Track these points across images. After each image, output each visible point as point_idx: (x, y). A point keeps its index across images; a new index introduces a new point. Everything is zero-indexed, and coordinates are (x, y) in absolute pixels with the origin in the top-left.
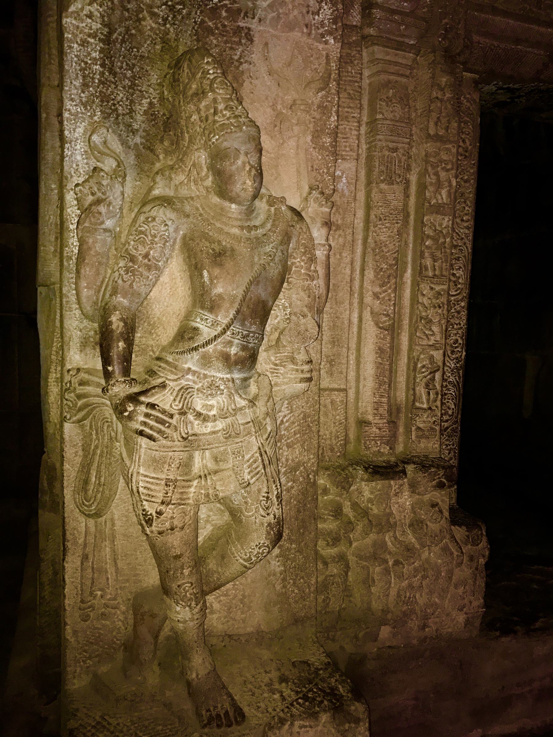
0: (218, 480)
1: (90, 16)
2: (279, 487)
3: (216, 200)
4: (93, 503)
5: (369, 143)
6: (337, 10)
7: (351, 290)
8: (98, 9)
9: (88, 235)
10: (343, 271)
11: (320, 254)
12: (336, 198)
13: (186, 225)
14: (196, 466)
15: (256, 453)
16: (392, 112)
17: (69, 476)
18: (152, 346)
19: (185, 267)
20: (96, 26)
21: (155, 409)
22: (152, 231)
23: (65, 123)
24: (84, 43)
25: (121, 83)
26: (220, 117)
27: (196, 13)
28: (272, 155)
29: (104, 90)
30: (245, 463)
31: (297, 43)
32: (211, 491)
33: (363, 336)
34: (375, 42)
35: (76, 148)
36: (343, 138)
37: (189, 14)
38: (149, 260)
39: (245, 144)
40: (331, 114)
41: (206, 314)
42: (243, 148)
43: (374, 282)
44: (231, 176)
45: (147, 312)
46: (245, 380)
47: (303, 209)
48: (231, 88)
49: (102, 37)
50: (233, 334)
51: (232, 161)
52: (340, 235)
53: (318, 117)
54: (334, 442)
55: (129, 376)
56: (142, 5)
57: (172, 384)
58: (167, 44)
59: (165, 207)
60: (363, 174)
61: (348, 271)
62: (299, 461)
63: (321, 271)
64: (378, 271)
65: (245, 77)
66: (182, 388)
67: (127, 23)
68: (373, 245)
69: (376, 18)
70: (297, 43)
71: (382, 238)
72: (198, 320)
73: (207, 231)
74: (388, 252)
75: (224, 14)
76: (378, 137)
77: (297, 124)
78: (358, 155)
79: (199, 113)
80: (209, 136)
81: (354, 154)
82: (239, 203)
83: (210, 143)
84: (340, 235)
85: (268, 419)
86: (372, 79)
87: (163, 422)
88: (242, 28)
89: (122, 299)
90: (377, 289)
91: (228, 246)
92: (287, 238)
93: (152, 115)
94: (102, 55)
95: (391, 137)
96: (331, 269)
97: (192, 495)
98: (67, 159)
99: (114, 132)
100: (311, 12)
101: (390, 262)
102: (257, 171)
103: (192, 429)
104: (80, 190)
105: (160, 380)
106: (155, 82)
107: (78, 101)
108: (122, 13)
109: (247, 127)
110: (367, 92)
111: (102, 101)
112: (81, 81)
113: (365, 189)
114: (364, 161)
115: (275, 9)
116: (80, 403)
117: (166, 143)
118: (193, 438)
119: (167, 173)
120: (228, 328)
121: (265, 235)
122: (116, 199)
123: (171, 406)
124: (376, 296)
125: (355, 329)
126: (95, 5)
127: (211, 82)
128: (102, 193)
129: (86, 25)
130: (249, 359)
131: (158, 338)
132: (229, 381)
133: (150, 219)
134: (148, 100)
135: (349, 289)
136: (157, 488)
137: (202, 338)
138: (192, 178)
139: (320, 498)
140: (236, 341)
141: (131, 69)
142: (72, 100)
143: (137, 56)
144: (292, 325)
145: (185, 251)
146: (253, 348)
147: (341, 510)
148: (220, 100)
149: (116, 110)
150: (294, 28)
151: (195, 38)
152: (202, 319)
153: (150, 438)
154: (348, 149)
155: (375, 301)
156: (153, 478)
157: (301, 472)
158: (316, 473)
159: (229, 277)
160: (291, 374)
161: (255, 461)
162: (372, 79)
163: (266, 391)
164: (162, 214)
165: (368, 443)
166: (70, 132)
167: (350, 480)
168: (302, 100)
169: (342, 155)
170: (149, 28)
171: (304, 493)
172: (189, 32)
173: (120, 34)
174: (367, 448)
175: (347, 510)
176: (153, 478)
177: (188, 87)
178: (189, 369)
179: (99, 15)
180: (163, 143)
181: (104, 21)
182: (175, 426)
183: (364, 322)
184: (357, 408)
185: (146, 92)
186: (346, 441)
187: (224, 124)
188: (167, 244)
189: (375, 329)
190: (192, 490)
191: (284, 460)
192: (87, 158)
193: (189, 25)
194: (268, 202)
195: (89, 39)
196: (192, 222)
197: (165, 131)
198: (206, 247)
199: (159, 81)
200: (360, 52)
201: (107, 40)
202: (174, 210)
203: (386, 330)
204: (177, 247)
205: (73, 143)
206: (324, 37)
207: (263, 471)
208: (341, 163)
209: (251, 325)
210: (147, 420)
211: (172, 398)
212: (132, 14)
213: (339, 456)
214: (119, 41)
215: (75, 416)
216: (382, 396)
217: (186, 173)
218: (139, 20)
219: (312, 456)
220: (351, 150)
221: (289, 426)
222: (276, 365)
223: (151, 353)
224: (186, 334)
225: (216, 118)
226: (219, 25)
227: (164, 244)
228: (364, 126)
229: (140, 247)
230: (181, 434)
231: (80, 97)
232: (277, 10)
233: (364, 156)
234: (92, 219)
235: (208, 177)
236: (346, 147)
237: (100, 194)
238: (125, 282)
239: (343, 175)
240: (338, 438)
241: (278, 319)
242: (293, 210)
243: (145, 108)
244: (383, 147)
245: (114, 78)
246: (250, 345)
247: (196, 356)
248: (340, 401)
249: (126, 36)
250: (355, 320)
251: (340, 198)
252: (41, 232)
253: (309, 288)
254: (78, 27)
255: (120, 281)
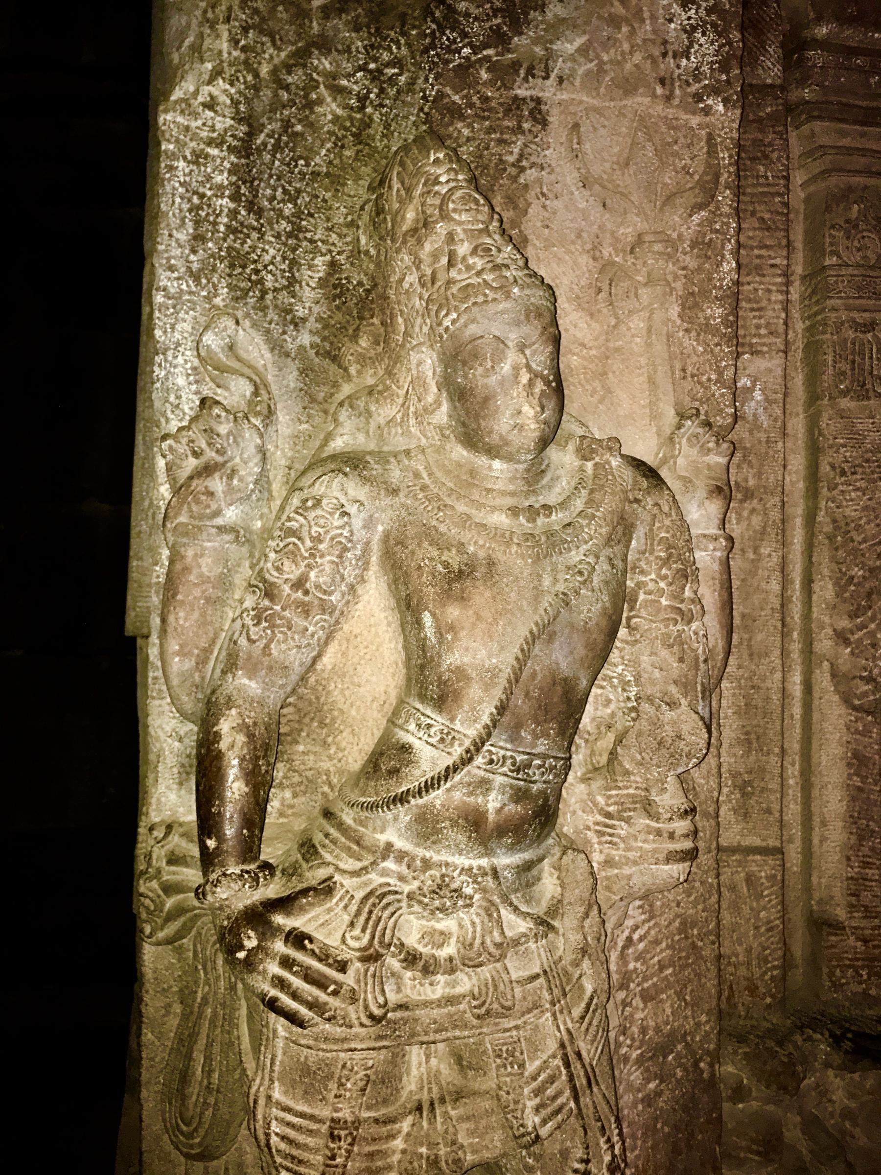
0: (461, 1119)
1: (211, 105)
2: (615, 1139)
3: (459, 452)
4: (196, 1130)
5: (809, 318)
6: (729, 43)
7: (783, 625)
8: (226, 91)
9: (185, 540)
10: (763, 585)
11: (706, 558)
12: (741, 432)
13: (390, 512)
14: (414, 1072)
15: (554, 1056)
16: (859, 250)
17: (152, 1059)
18: (328, 773)
19: (393, 603)
20: (223, 123)
21: (303, 948)
22: (315, 529)
23: (157, 314)
24: (198, 158)
25: (272, 229)
26: (460, 272)
27: (426, 80)
28: (593, 352)
29: (237, 245)
30: (528, 1083)
31: (642, 119)
32: (443, 1151)
33: (815, 728)
34: (815, 113)
35: (175, 362)
36: (752, 310)
37: (412, 82)
38: (306, 593)
39: (518, 325)
40: (723, 256)
41: (428, 712)
42: (513, 336)
43: (835, 607)
44: (486, 400)
45: (317, 698)
46: (528, 866)
47: (664, 461)
48: (486, 209)
49: (235, 143)
50: (491, 762)
51: (490, 364)
52: (753, 511)
53: (693, 264)
54: (757, 972)
55: (256, 858)
56: (314, 75)
57: (348, 882)
58: (368, 145)
59: (345, 474)
60: (798, 381)
61: (775, 586)
62: (673, 1031)
63: (710, 597)
64: (843, 583)
65: (531, 195)
66: (371, 893)
67: (286, 112)
68: (828, 529)
69: (815, 66)
70: (642, 119)
71: (848, 512)
72: (412, 727)
73: (434, 523)
74: (865, 541)
75: (484, 75)
76: (830, 303)
77: (646, 285)
78: (787, 343)
79: (418, 268)
80: (437, 316)
81: (779, 342)
82: (509, 458)
83: (441, 330)
84: (753, 511)
85: (586, 964)
86: (812, 188)
87: (320, 983)
88: (524, 99)
89: (245, 681)
90: (844, 623)
91: (482, 554)
92: (622, 529)
93: (335, 287)
94: (234, 179)
95: (858, 302)
96: (736, 583)
97: (396, 1157)
98: (158, 385)
99: (254, 325)
100: (670, 53)
101: (871, 563)
102: (548, 383)
103: (399, 990)
104: (171, 448)
105: (322, 873)
106: (341, 220)
107: (183, 270)
108: (276, 95)
109: (522, 288)
110: (802, 217)
111: (232, 266)
112: (191, 231)
113: (806, 411)
114: (799, 355)
115: (591, 54)
116: (170, 903)
117: (364, 342)
118: (399, 1014)
119: (361, 403)
120: (478, 750)
121: (569, 524)
122: (245, 463)
123: (343, 941)
124: (842, 637)
125: (797, 710)
126: (221, 81)
127: (443, 200)
128: (217, 451)
129: (204, 124)
130: (539, 816)
131: (340, 755)
132: (485, 874)
133: (310, 504)
134: (328, 257)
135: (779, 624)
136: (310, 1141)
137: (417, 772)
138: (412, 409)
139: (726, 1106)
140: (499, 780)
141: (293, 200)
142: (172, 269)
143: (304, 174)
144: (643, 724)
145: (389, 567)
146: (543, 793)
147: (779, 1136)
148: (462, 236)
149: (261, 281)
150: (636, 90)
151: (424, 128)
152: (419, 726)
153: (293, 1018)
154: (763, 331)
155: (840, 649)
156: (302, 1115)
157: (678, 1057)
158: (716, 1058)
159: (482, 626)
160: (645, 841)
161: (552, 1080)
162: (812, 188)
163: (580, 891)
164: (334, 489)
165: (838, 972)
166: (165, 332)
167: (799, 1068)
168: (655, 233)
169: (751, 345)
170: (330, 117)
171: (689, 1105)
172: (413, 118)
173: (269, 136)
174: (837, 986)
175: (793, 1134)
176: (302, 1115)
177: (399, 219)
178: (389, 846)
179: (228, 102)
180: (357, 343)
181: (238, 112)
182: (353, 991)
183: (816, 695)
184: (808, 889)
185: (323, 242)
186: (787, 963)
187: (468, 285)
188: (349, 555)
189: (843, 710)
190: (399, 1143)
191: (635, 1030)
192: (197, 382)
193: (412, 105)
194: (578, 450)
195: (209, 150)
196: (403, 505)
197: (361, 318)
198: (431, 559)
199: (349, 218)
200: (783, 136)
201: (245, 148)
202: (366, 480)
203: (869, 713)
204: (374, 559)
205: (170, 353)
206: (701, 100)
207: (572, 1104)
208: (750, 361)
209: (536, 737)
210: (286, 974)
211: (347, 918)
212: (296, 94)
213: (769, 1006)
214: (269, 147)
215: (162, 929)
216: (866, 865)
217: (400, 401)
218: (310, 105)
219: (704, 1018)
220: (771, 333)
221: (646, 951)
222: (608, 815)
223: (326, 789)
224: (388, 759)
225: (453, 274)
226: (475, 99)
227: (340, 556)
228: (797, 283)
229: (287, 566)
230: (366, 1007)
231: (187, 261)
232: (598, 57)
233: (799, 344)
234: (195, 508)
235: (440, 405)
236: (758, 327)
237: (214, 454)
238: (254, 642)
239: (754, 386)
240: (766, 961)
241: (613, 706)
242: (638, 464)
243: (321, 274)
244: (842, 323)
245: (257, 220)
246: (535, 788)
247: (404, 814)
248: (767, 877)
249: (285, 138)
250: (797, 690)
251: (751, 432)
252: (133, 533)
253: (680, 640)
254: (187, 129)
255: (243, 641)
